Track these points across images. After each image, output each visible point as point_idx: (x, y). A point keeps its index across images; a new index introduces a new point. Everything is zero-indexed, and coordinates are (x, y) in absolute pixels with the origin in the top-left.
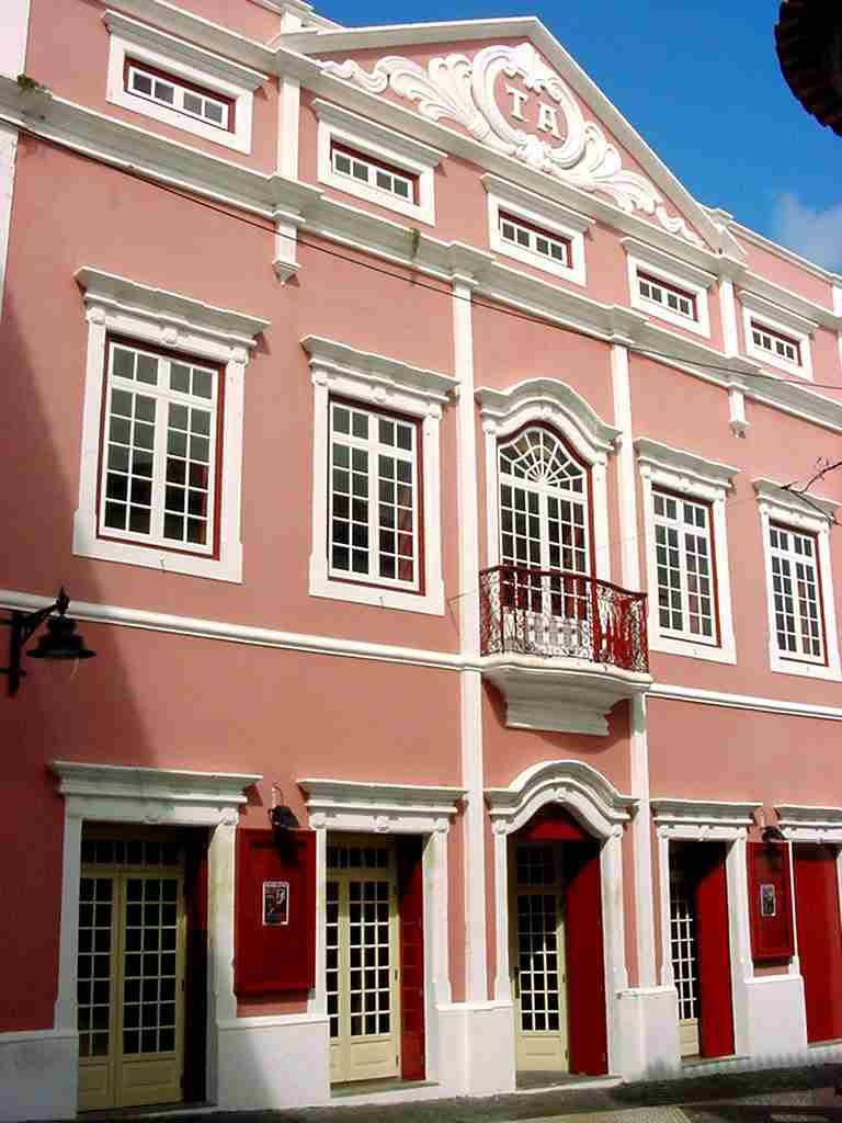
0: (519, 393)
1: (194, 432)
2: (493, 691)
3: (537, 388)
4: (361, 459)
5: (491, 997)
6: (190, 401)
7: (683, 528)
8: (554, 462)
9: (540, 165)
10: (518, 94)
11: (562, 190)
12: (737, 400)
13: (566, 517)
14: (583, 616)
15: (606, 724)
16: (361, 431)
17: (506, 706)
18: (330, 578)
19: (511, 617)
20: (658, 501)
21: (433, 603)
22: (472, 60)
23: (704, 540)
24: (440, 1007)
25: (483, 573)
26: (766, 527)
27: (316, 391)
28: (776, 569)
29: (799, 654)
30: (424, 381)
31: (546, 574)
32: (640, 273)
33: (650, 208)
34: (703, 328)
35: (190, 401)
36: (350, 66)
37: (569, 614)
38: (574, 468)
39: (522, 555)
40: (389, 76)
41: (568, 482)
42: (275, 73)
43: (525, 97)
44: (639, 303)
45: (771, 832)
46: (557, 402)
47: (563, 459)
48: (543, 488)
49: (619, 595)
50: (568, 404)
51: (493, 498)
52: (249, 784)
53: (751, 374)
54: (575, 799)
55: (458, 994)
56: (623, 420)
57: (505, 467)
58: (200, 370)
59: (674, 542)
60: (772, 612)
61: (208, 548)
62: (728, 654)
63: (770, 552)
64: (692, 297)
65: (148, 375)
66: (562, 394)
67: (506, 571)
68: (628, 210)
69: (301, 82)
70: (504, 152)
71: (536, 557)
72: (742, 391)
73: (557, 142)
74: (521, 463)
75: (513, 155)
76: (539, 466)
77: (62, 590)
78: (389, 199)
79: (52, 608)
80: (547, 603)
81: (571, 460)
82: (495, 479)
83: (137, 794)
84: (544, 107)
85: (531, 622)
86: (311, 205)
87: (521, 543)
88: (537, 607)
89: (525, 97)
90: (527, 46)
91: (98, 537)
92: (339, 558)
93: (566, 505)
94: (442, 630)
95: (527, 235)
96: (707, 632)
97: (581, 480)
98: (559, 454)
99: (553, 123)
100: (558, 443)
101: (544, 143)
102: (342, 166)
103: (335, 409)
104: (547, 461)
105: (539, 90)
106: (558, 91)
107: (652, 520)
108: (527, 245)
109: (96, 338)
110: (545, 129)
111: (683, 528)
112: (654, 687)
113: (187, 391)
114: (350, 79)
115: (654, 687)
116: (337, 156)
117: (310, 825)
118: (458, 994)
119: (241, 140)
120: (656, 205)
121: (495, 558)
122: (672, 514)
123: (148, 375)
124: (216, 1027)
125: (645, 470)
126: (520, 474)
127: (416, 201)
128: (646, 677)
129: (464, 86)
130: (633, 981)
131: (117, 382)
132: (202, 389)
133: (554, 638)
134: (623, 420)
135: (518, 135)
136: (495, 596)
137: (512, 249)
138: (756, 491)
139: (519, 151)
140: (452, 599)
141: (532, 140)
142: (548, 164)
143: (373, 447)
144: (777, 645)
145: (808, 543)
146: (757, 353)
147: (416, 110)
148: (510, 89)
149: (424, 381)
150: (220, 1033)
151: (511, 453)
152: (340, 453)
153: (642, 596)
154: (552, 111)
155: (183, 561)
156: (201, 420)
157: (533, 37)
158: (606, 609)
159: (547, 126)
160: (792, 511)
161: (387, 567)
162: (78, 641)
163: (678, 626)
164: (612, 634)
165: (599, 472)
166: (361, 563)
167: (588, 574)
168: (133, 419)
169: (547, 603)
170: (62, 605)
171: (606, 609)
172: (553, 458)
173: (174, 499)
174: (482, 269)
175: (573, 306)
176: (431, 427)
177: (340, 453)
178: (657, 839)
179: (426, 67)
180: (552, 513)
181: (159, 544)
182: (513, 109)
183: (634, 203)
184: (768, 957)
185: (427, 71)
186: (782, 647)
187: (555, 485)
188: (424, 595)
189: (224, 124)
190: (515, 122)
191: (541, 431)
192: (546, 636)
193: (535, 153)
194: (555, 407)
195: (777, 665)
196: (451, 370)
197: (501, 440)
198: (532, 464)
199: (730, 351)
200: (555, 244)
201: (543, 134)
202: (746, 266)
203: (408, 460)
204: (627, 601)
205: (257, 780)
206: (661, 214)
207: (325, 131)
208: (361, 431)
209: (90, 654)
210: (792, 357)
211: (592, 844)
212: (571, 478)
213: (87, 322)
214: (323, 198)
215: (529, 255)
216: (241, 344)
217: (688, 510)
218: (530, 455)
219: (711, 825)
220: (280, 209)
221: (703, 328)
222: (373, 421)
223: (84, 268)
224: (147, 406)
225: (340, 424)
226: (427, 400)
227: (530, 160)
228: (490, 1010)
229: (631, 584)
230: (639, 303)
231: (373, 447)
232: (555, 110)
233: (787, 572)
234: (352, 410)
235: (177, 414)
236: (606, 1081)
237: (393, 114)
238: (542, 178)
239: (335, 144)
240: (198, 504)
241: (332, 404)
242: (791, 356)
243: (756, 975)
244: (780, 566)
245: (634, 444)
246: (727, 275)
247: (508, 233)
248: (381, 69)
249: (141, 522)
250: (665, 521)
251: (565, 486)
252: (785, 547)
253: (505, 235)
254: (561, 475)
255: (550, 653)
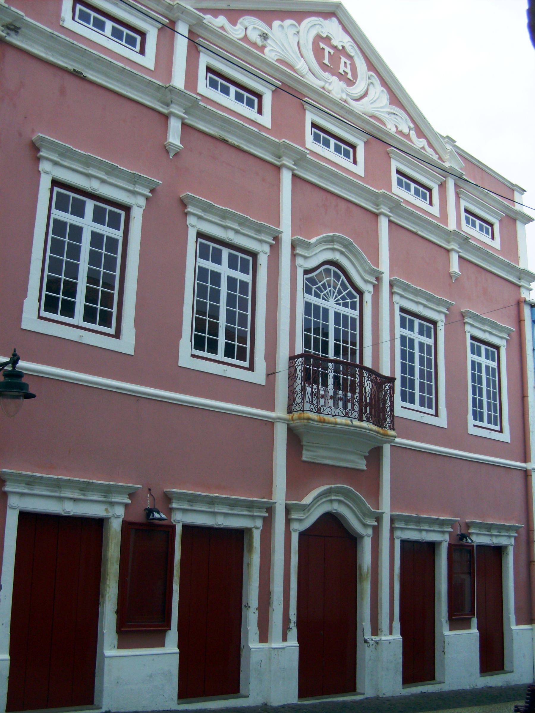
0: (319, 243)
1: (108, 254)
2: (295, 439)
3: (332, 240)
4: (216, 277)
5: (285, 639)
6: (106, 231)
7: (418, 338)
8: (339, 289)
9: (339, 96)
10: (327, 49)
11: (351, 112)
12: (454, 258)
13: (345, 326)
14: (353, 392)
15: (365, 462)
16: (217, 260)
17: (302, 447)
18: (192, 356)
19: (309, 389)
20: (403, 320)
21: (258, 376)
22: (299, 24)
23: (355, 319)
24: (251, 645)
25: (292, 358)
26: (469, 341)
27: (189, 229)
28: (473, 368)
29: (417, 406)
30: (260, 229)
31: (331, 361)
32: (398, 172)
33: (406, 131)
34: (435, 210)
35: (106, 231)
36: (221, 20)
37: (345, 390)
38: (353, 294)
39: (316, 348)
40: (246, 29)
41: (348, 302)
42: (173, 19)
43: (332, 52)
44: (398, 191)
45: (463, 536)
46: (344, 250)
47: (345, 288)
48: (332, 306)
49: (378, 378)
50: (350, 251)
51: (398, 342)
52: (133, 491)
53: (465, 240)
54: (337, 508)
55: (264, 637)
56: (384, 266)
57: (308, 290)
58: (113, 212)
59: (412, 347)
60: (470, 396)
61: (112, 331)
62: (442, 421)
63: (470, 357)
64: (492, 225)
65: (79, 211)
66: (347, 245)
67: (306, 356)
68: (393, 130)
69: (190, 26)
70: (273, 59)
71: (325, 350)
72: (458, 252)
73: (350, 83)
74: (319, 288)
75: (323, 88)
76: (330, 291)
77: (15, 351)
78: (242, 109)
79: (6, 364)
80: (331, 381)
81: (350, 288)
82: (301, 297)
83: (57, 494)
84: (343, 60)
85: (322, 392)
86: (193, 105)
87: (316, 340)
88: (325, 384)
89: (332, 52)
90: (334, 19)
91: (40, 317)
92: (199, 343)
93: (345, 317)
94: (264, 395)
95: (329, 141)
96: (430, 407)
97: (356, 302)
98: (343, 284)
99: (348, 70)
100: (343, 277)
101: (342, 82)
102: (213, 84)
103: (201, 243)
104: (335, 288)
105: (341, 48)
106: (352, 51)
107: (399, 331)
108: (329, 147)
109: (45, 183)
110: (343, 74)
111: (418, 338)
112: (397, 440)
113: (208, 260)
114: (222, 28)
115: (397, 440)
116: (210, 78)
117: (172, 521)
118: (264, 637)
119: (149, 61)
120: (410, 129)
121: (299, 349)
122: (412, 329)
123: (79, 211)
124: (103, 656)
125: (396, 298)
126: (317, 295)
127: (260, 112)
128: (393, 433)
129: (294, 41)
130: (375, 631)
131: (58, 214)
132: (114, 224)
133: (336, 406)
134: (384, 266)
135: (327, 75)
136: (299, 373)
137: (319, 149)
138: (463, 317)
139: (327, 86)
140: (271, 374)
141: (335, 79)
142: (344, 97)
143: (224, 270)
144: (472, 417)
145: (429, 329)
146: (467, 229)
147: (263, 53)
148: (322, 45)
149: (260, 229)
150: (107, 661)
151: (312, 281)
152: (202, 273)
153: (392, 380)
154: (348, 62)
155: (96, 338)
156: (112, 243)
157: (339, 13)
158: (368, 387)
159: (344, 71)
160: (485, 331)
161: (229, 352)
162: (23, 387)
163: (412, 401)
164: (373, 403)
165: (368, 298)
166: (213, 347)
167: (358, 362)
168: (67, 240)
169: (331, 381)
170: (14, 361)
171: (368, 387)
172: (339, 286)
173: (91, 295)
174: (301, 159)
175: (257, 139)
176: (263, 260)
177: (202, 273)
178: (394, 539)
179: (270, 26)
180: (337, 322)
181: (80, 325)
182: (323, 58)
183: (396, 127)
184: (457, 620)
185: (271, 29)
186: (475, 419)
187: (339, 304)
188: (119, 338)
189: (138, 49)
190: (324, 67)
191: (333, 268)
192: (331, 403)
193: (336, 88)
194: (342, 253)
195: (472, 430)
196: (277, 223)
197: (306, 272)
198: (325, 289)
199: (452, 226)
200: (347, 148)
201: (342, 77)
202: (464, 173)
203: (431, 344)
204: (383, 382)
205: (138, 489)
206: (413, 134)
207: (204, 60)
208: (217, 260)
209: (32, 396)
210: (488, 234)
211: (352, 541)
212: (350, 301)
213: (39, 172)
214: (308, 156)
215: (330, 153)
216: (505, 338)
217: (421, 326)
218: (324, 283)
219: (226, 515)
220: (453, 245)
221: (435, 210)
222: (225, 253)
223: (40, 134)
224: (77, 232)
225: (203, 253)
226: (261, 241)
227: (333, 92)
228: (284, 648)
229: (386, 372)
230: (398, 191)
231: (224, 270)
232: (350, 62)
233: (480, 371)
234: (212, 244)
235: (96, 238)
236: (437, 686)
237: (248, 54)
238: (341, 106)
239: (209, 70)
240: (107, 300)
241: (200, 240)
242: (487, 233)
243: (121, 646)
244: (477, 366)
245: (291, 240)
246: (185, 22)
247: (317, 138)
248: (241, 23)
249: (69, 309)
250: (476, 358)
251: (346, 305)
252: (479, 355)
253: (315, 139)
254: (343, 298)
255: (333, 414)
